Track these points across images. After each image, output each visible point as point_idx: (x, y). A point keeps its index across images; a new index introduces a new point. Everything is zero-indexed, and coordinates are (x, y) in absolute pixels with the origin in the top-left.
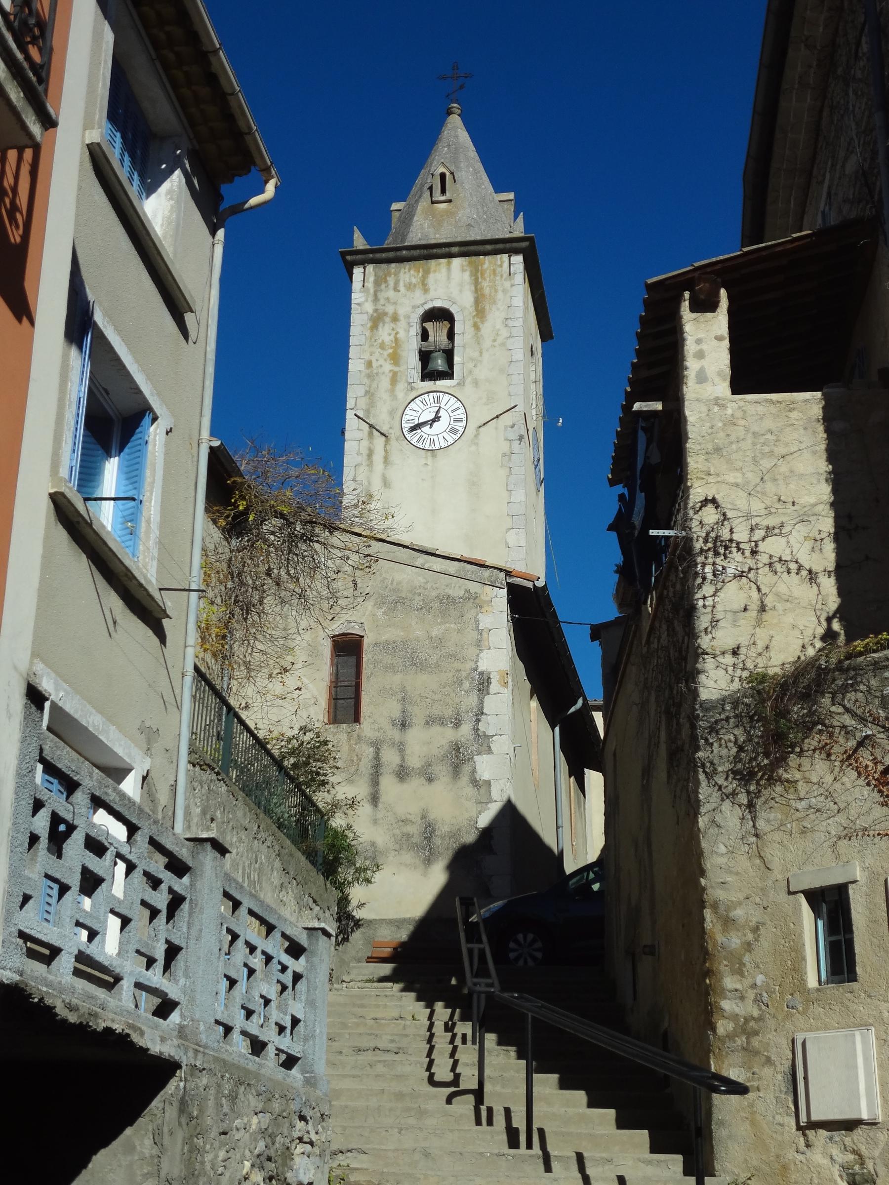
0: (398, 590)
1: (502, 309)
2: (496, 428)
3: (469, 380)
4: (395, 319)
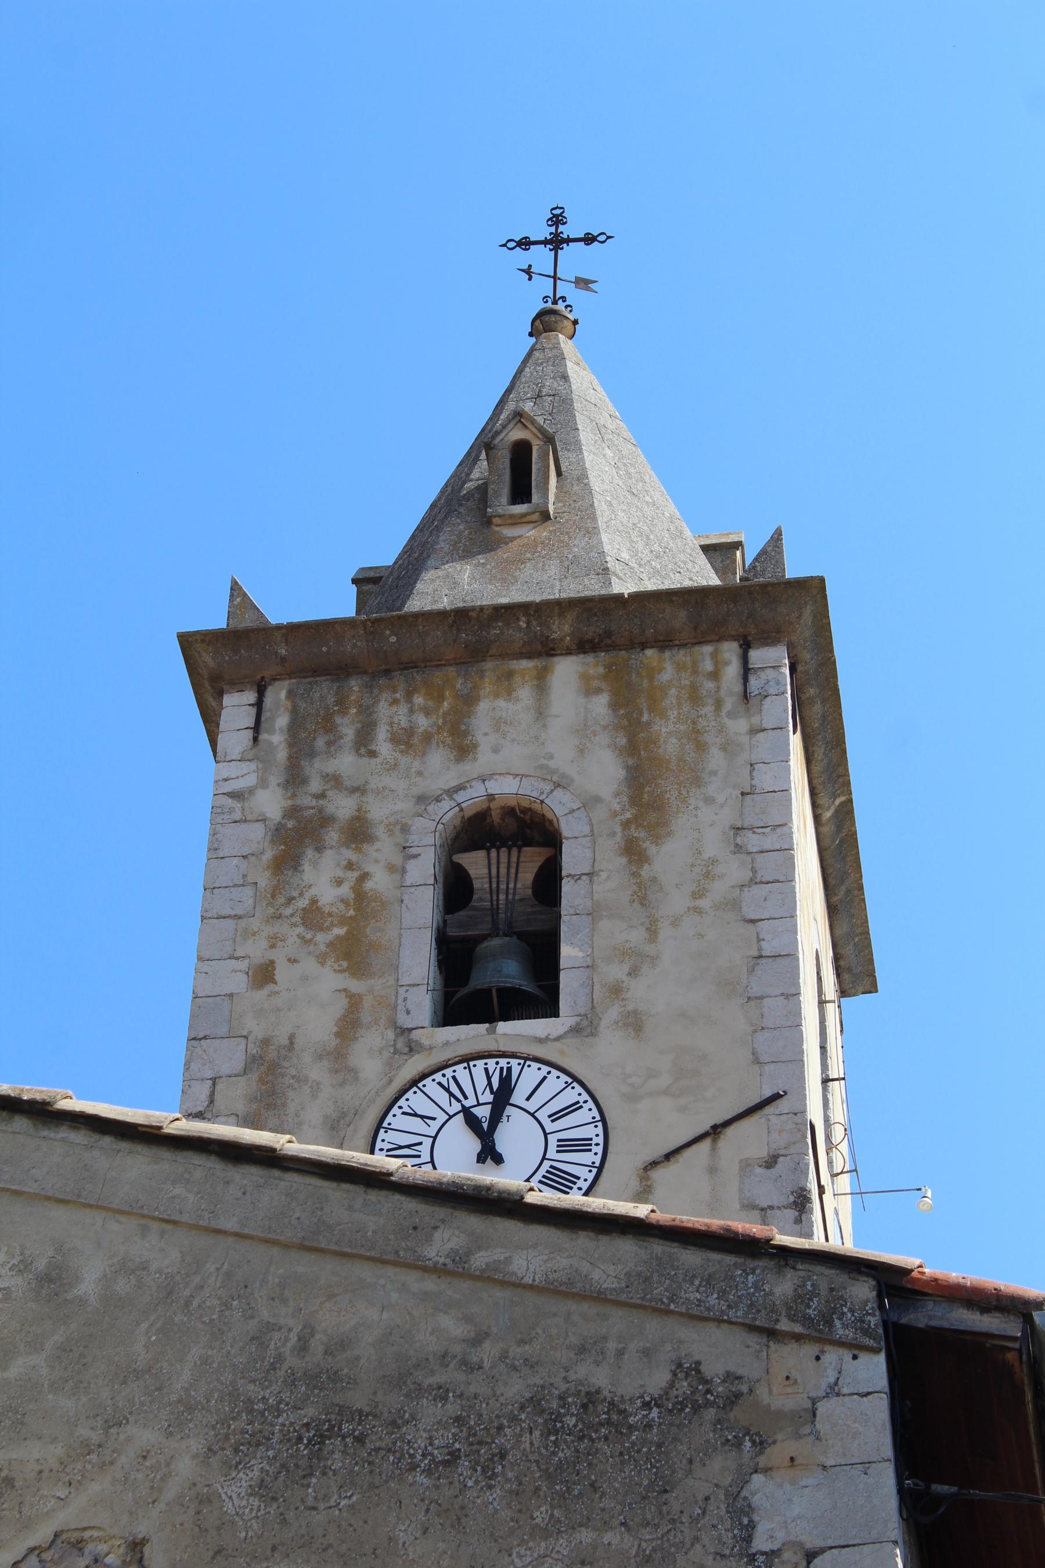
0: (335, 1376)
1: (721, 799)
3: (613, 1014)
4: (358, 832)
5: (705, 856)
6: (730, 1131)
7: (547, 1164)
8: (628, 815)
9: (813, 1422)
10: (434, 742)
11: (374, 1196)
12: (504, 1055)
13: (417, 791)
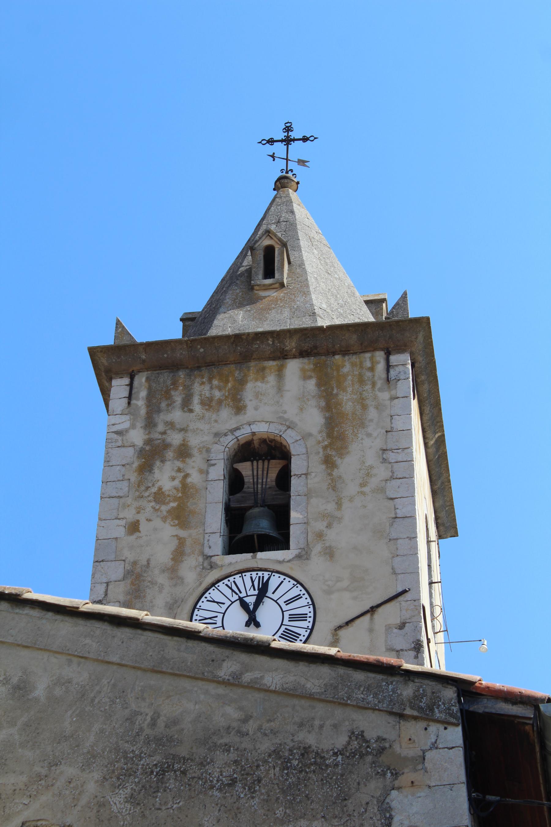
0: (170, 739)
1: (375, 434)
2: (371, 630)
3: (317, 548)
4: (184, 452)
6: (380, 610)
7: (283, 628)
8: (326, 443)
9: (423, 763)
10: (223, 404)
11: (191, 644)
13: (214, 430)
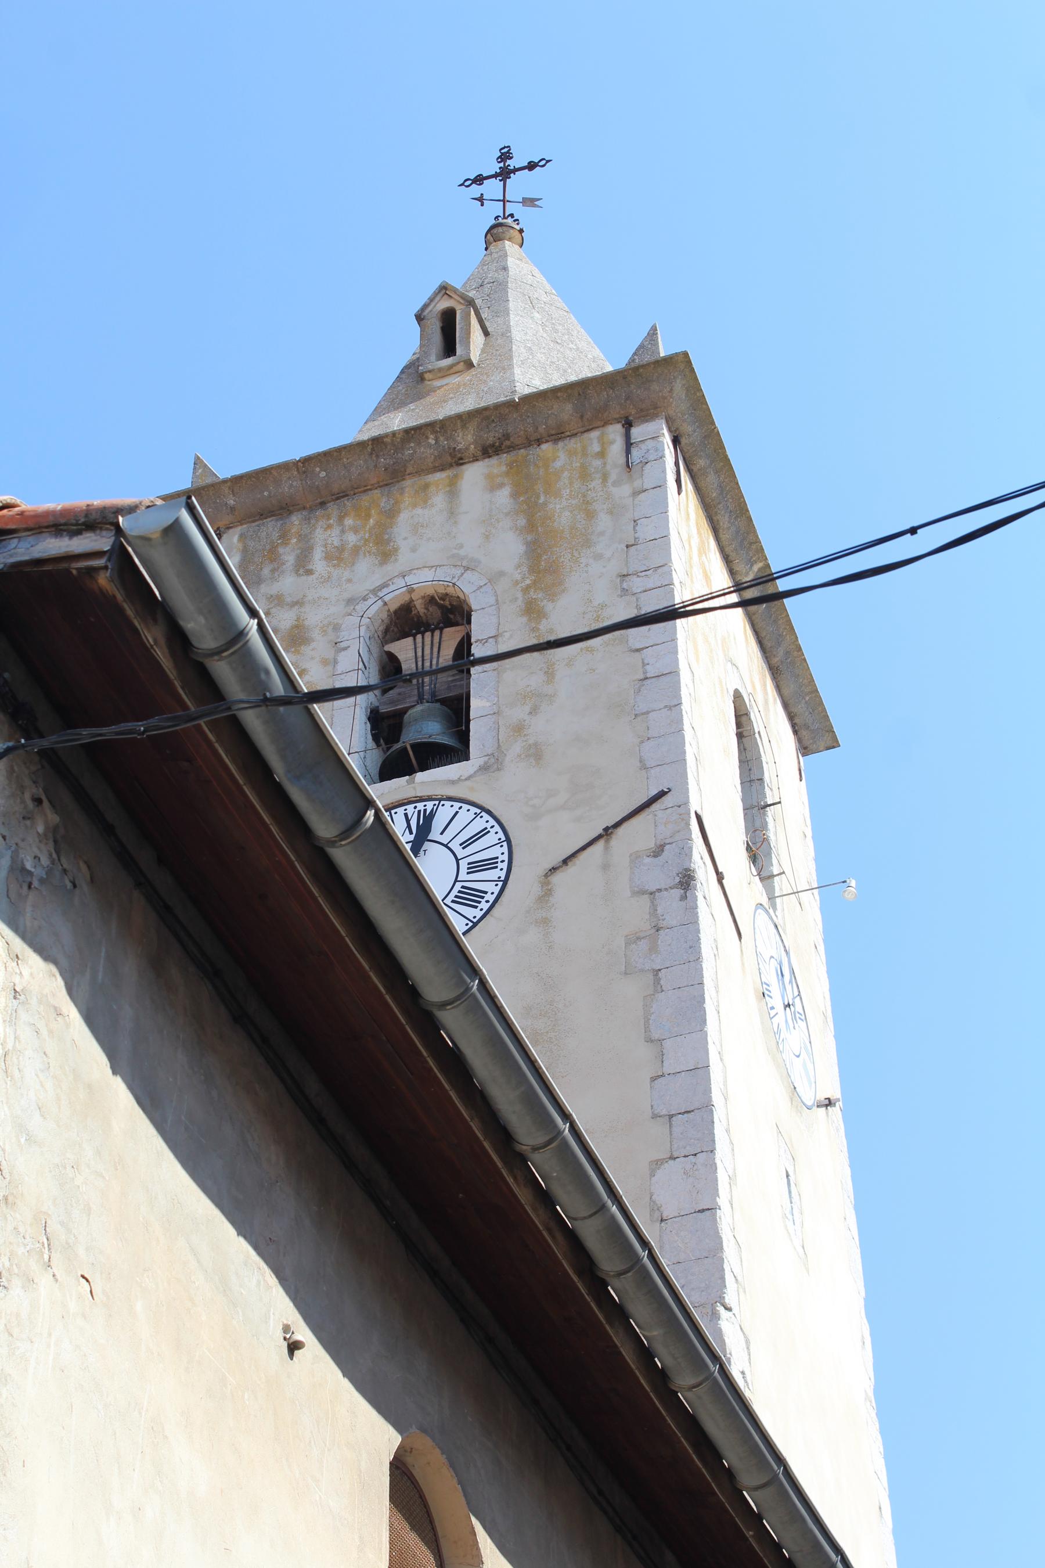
5: (596, 603)
6: (621, 831)
7: (458, 886)
8: (528, 582)
10: (361, 553)
12: (421, 800)
13: (346, 595)
